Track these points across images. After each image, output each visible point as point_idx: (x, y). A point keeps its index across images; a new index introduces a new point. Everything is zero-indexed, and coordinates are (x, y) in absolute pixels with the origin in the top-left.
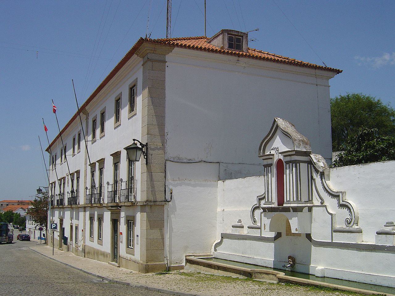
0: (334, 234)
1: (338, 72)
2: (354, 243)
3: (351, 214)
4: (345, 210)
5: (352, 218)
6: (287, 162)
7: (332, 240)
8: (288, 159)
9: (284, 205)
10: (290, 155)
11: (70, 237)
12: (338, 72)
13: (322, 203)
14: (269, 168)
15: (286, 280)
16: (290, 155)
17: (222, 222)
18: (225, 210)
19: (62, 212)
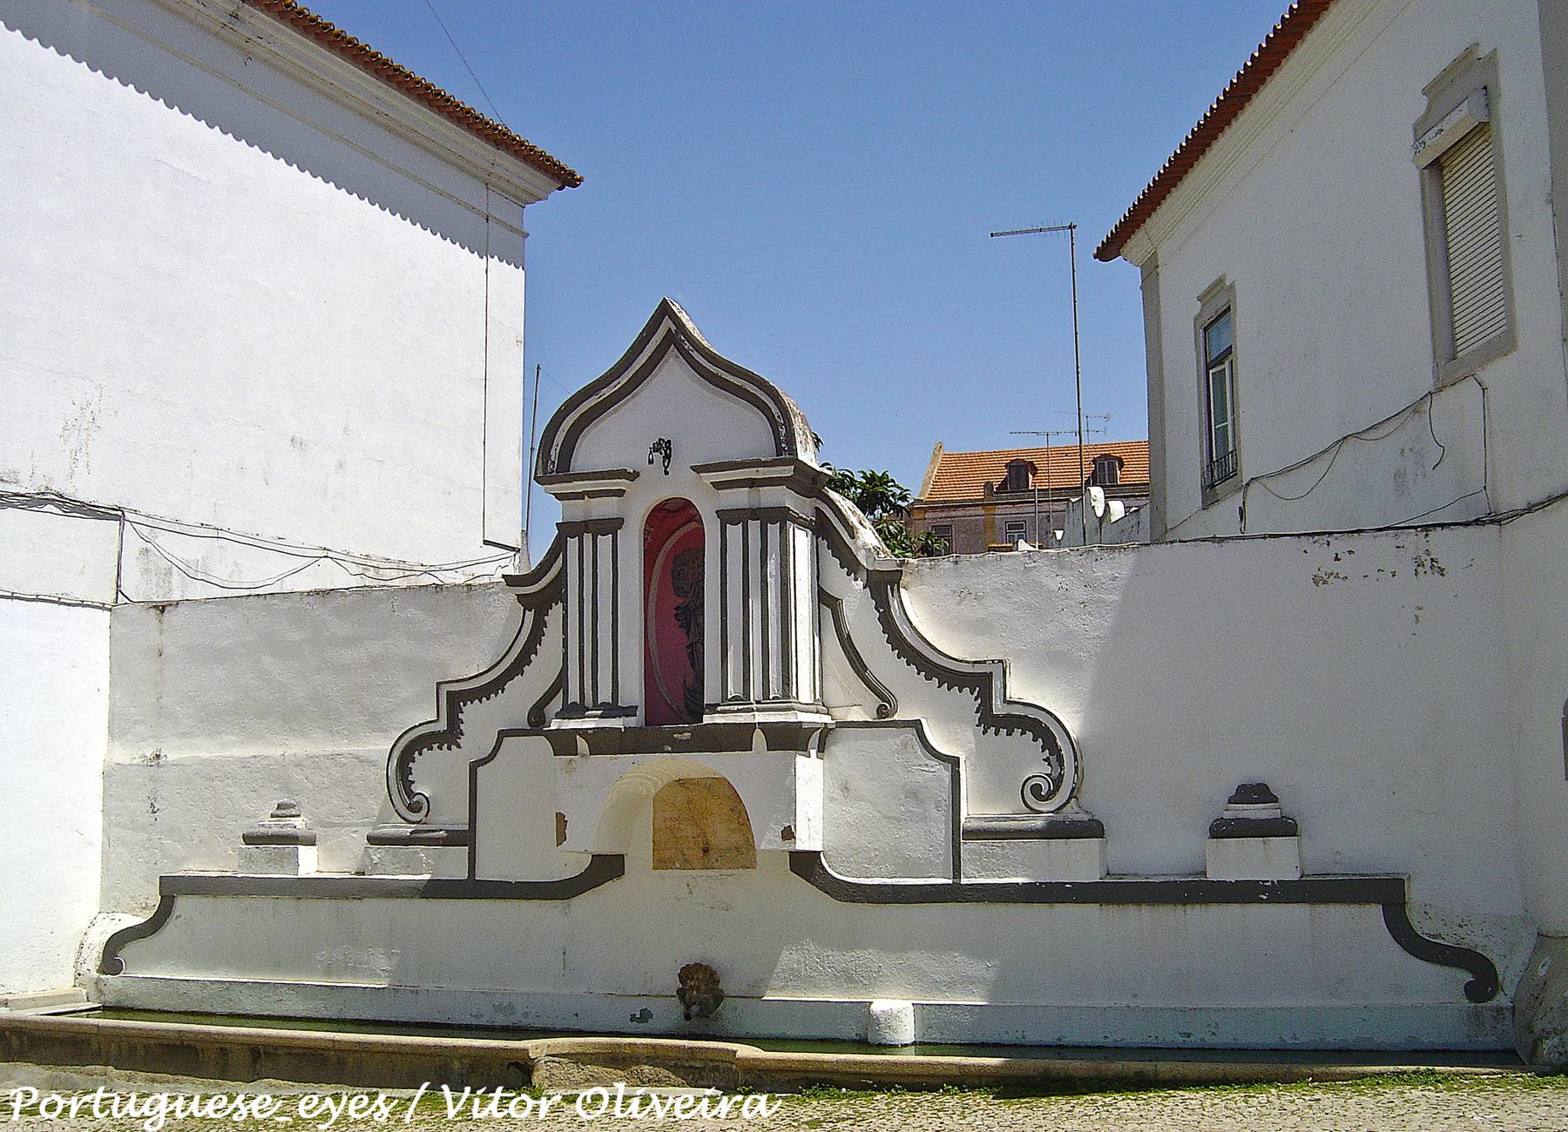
0: (967, 847)
1: (566, 179)
2: (1020, 880)
3: (1053, 759)
4: (1024, 743)
5: (1061, 776)
6: (727, 517)
7: (957, 872)
8: (739, 498)
9: (707, 719)
10: (752, 483)
11: (1204, 1060)
12: (566, 179)
13: (881, 712)
14: (605, 542)
15: (802, 1075)
16: (752, 483)
17: (149, 818)
18: (171, 756)
19: (978, 689)
